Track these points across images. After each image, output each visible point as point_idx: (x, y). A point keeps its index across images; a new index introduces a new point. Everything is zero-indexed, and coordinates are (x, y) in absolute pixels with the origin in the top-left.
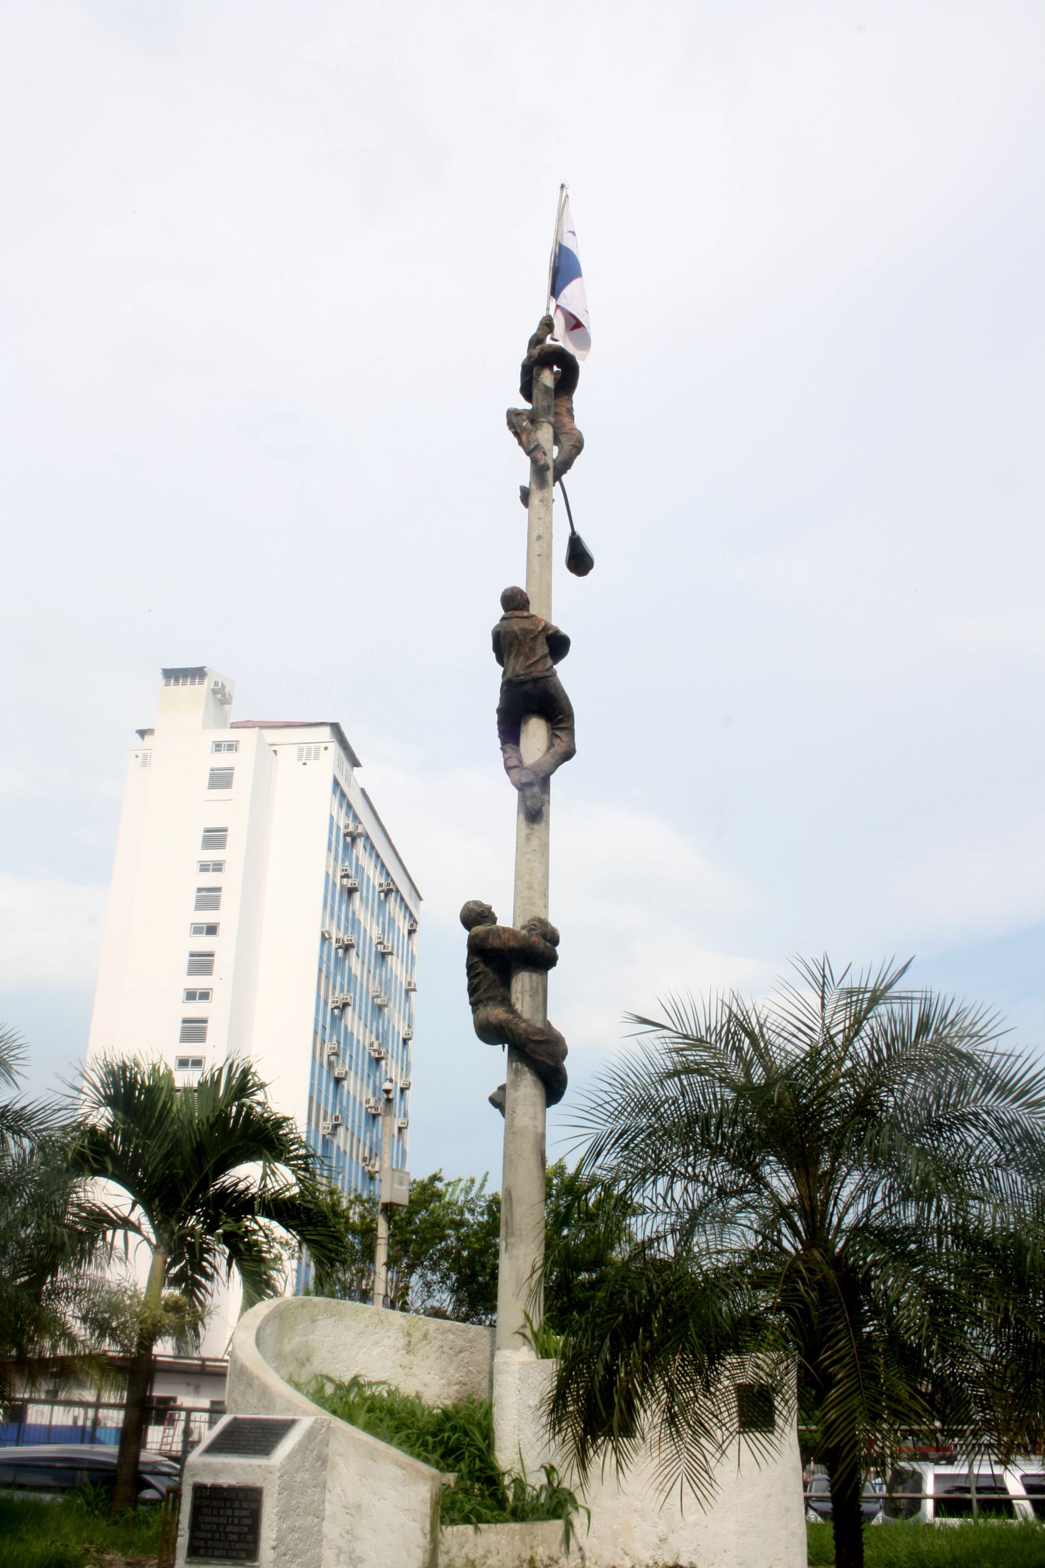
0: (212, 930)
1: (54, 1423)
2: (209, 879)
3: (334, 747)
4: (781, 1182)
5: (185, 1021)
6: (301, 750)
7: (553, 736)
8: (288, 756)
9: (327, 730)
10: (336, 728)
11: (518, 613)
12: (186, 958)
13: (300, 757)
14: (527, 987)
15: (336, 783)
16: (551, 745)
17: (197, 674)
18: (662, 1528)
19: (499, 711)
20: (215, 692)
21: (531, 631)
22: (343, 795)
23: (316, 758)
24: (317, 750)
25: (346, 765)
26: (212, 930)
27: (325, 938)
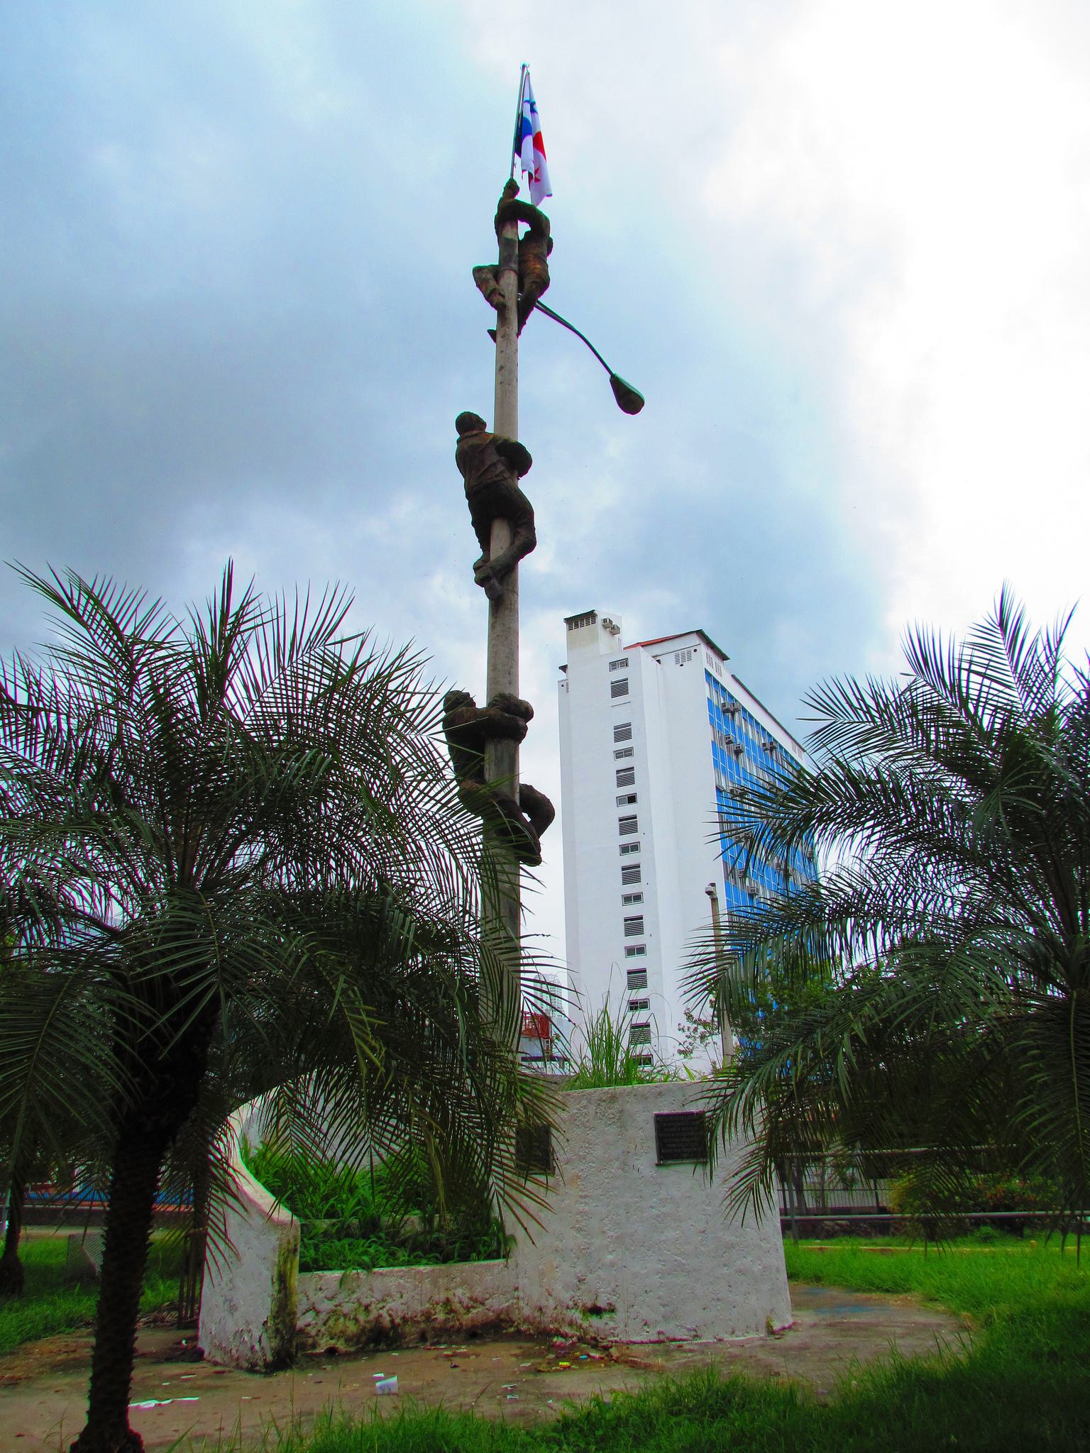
0: (632, 799)
1: (692, 1167)
2: (624, 763)
3: (703, 649)
4: (791, 895)
5: (623, 869)
6: (677, 656)
7: (514, 534)
8: (669, 660)
9: (695, 640)
10: (700, 633)
11: (469, 434)
12: (617, 824)
13: (677, 662)
14: (493, 758)
15: (708, 674)
16: (512, 543)
17: (590, 616)
18: (580, 1269)
19: (473, 524)
20: (605, 627)
21: (479, 446)
22: (716, 682)
23: (690, 659)
24: (689, 653)
25: (715, 659)
26: (632, 799)
27: (719, 790)
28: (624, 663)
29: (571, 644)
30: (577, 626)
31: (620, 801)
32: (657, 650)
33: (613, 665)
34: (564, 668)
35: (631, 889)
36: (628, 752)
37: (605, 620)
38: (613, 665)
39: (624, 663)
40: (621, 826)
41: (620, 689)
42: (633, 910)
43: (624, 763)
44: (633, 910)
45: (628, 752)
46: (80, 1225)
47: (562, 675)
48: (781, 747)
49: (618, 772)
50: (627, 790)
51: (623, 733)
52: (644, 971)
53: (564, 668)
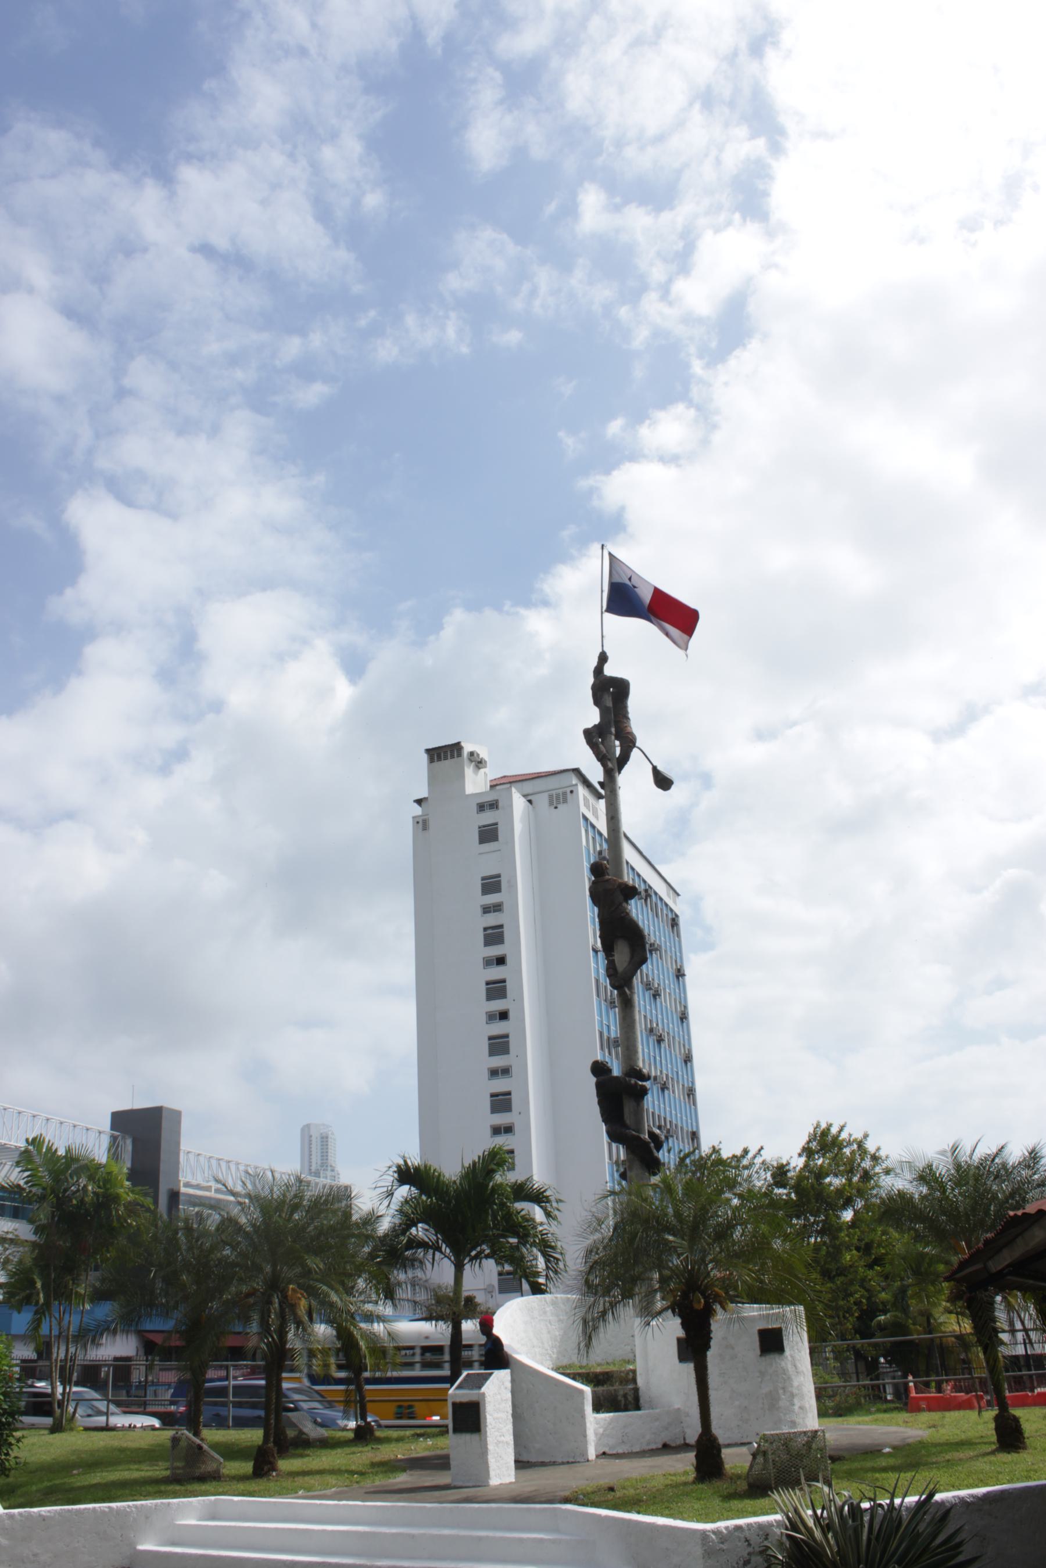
2: (492, 920)
5: (488, 983)
6: (551, 797)
8: (542, 801)
10: (577, 772)
13: (551, 803)
17: (455, 749)
23: (565, 801)
24: (565, 794)
28: (494, 805)
29: (433, 779)
30: (439, 759)
31: (488, 962)
32: (529, 787)
33: (481, 807)
34: (419, 802)
35: (498, 1062)
36: (497, 908)
37: (472, 754)
38: (481, 807)
39: (494, 805)
40: (487, 990)
41: (488, 834)
42: (500, 1085)
43: (492, 920)
44: (500, 1085)
45: (497, 908)
46: (947, 1511)
47: (418, 810)
48: (656, 894)
49: (485, 929)
50: (498, 1005)
51: (491, 885)
52: (504, 981)
53: (419, 802)
